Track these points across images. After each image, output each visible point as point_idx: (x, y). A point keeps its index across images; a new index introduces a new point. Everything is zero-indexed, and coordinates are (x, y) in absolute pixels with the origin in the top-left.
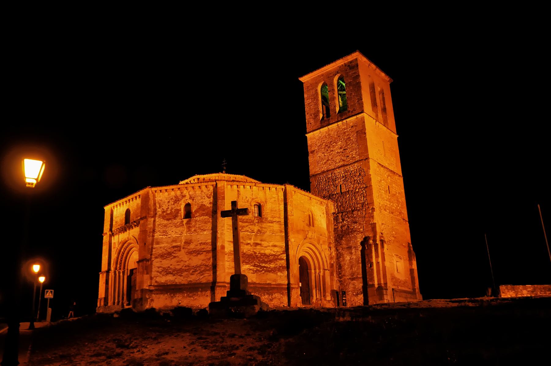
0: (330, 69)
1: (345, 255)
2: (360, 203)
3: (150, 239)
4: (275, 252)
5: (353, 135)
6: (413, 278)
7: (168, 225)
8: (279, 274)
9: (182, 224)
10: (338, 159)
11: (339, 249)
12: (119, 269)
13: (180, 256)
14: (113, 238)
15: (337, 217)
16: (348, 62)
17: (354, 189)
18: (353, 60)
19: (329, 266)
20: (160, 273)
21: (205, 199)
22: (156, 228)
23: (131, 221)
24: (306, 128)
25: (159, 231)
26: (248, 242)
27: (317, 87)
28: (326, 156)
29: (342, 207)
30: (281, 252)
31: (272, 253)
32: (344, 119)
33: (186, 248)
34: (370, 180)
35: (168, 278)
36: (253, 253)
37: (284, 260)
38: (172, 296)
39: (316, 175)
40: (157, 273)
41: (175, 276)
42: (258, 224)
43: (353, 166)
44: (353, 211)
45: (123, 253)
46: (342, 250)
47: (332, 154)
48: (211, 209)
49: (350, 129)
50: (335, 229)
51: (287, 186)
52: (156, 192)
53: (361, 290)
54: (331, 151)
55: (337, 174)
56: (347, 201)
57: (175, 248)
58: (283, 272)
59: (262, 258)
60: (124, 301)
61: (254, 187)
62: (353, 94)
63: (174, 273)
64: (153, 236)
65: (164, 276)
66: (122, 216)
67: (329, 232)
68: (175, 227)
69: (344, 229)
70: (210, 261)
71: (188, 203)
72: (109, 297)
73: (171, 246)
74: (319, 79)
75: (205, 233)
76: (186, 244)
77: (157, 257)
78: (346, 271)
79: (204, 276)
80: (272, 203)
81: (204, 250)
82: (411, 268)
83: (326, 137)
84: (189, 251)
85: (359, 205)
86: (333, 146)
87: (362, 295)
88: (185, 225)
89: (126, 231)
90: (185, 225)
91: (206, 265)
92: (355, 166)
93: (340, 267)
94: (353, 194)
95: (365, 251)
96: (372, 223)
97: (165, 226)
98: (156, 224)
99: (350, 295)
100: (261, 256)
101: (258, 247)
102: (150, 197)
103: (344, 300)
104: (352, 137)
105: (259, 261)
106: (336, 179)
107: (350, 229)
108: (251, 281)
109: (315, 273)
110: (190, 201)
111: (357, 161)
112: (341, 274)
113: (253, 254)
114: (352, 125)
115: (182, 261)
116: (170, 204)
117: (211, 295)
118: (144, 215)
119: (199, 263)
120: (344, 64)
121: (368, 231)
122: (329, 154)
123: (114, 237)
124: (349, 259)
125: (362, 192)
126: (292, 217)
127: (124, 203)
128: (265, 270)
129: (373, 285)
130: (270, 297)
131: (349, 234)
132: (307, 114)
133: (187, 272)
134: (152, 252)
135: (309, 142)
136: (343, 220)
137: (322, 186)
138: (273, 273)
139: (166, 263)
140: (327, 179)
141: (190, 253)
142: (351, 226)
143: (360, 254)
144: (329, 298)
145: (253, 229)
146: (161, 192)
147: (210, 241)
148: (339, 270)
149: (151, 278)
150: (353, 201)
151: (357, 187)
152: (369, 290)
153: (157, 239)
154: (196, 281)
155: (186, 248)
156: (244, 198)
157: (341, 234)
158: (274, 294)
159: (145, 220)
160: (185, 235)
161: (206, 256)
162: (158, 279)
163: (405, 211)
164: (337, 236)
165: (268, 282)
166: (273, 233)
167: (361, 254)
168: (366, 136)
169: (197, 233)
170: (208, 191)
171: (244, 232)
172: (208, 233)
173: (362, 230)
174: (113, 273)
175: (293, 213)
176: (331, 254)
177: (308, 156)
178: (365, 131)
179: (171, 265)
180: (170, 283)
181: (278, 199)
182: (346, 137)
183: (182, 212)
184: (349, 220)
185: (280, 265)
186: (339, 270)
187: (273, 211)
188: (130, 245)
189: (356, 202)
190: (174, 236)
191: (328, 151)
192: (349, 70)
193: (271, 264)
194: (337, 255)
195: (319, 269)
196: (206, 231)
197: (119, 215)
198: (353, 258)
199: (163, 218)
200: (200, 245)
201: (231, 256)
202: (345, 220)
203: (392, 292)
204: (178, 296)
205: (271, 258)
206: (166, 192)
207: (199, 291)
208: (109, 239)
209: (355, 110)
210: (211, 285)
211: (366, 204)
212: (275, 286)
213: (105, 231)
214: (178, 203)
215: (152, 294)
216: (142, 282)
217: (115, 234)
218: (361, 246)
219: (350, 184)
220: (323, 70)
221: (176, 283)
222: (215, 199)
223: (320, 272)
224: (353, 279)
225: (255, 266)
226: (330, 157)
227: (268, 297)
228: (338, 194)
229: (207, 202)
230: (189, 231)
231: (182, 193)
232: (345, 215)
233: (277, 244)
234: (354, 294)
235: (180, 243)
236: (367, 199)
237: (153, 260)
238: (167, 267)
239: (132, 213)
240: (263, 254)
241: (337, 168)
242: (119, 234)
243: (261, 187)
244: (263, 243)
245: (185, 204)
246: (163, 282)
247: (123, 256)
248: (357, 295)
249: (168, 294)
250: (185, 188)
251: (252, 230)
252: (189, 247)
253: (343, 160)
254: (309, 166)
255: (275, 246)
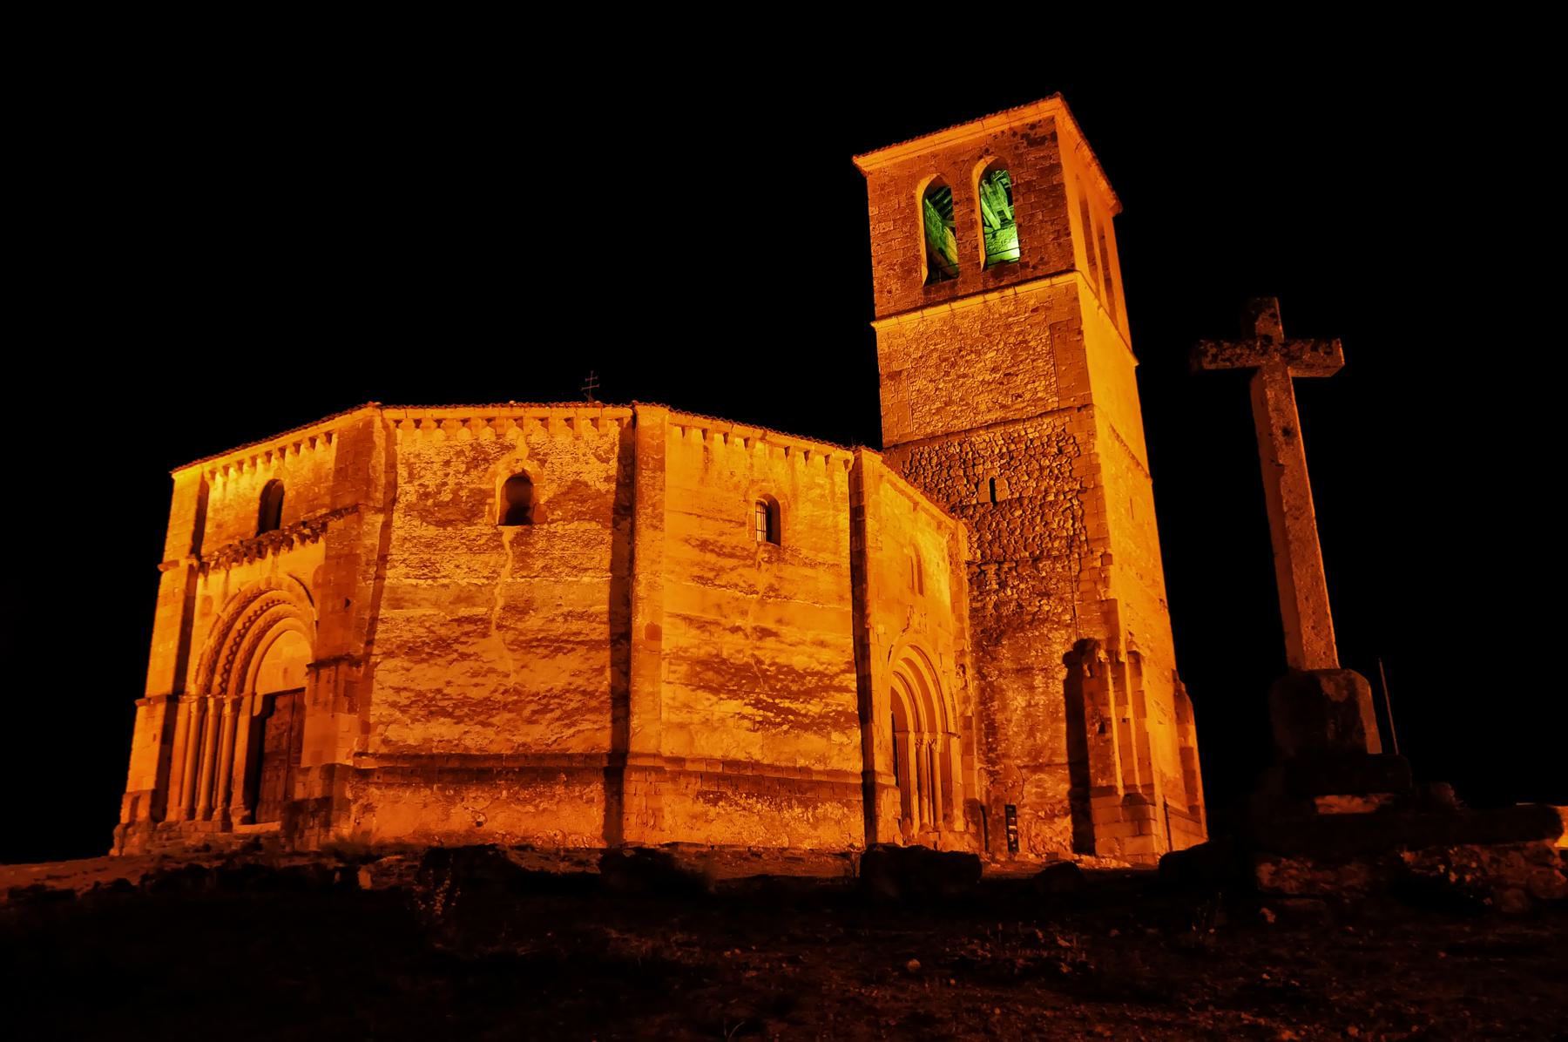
0: (960, 141)
1: (1010, 694)
2: (1062, 538)
3: (367, 587)
4: (822, 664)
5: (1038, 335)
6: (1188, 774)
7: (440, 541)
8: (836, 737)
9: (496, 544)
10: (984, 401)
11: (989, 674)
12: (219, 689)
13: (484, 655)
14: (200, 581)
15: (980, 574)
16: (1023, 125)
17: (1039, 492)
18: (1040, 121)
19: (960, 724)
20: (404, 710)
21: (587, 463)
22: (392, 551)
23: (286, 522)
24: (872, 305)
25: (405, 560)
26: (737, 624)
27: (915, 187)
28: (941, 389)
29: (997, 544)
30: (843, 667)
31: (812, 666)
32: (1008, 287)
33: (508, 628)
34: (1096, 469)
35: (434, 731)
36: (752, 661)
37: (852, 691)
38: (448, 797)
39: (904, 444)
40: (391, 711)
41: (462, 725)
42: (768, 566)
43: (1035, 424)
44: (1036, 560)
45: (242, 636)
46: (1000, 675)
47: (962, 385)
48: (611, 498)
49: (1027, 315)
50: (973, 611)
51: (866, 454)
52: (397, 426)
53: (1066, 803)
54: (959, 377)
55: (981, 447)
56: (1016, 529)
57: (465, 626)
58: (847, 732)
59: (782, 680)
60: (231, 808)
61: (759, 445)
62: (1041, 218)
63: (458, 713)
64: (380, 578)
65: (419, 720)
66: (248, 504)
67: (960, 619)
68: (471, 550)
69: (1005, 611)
70: (602, 677)
71: (524, 471)
72: (174, 791)
73: (448, 618)
74: (922, 166)
75: (586, 579)
76: (509, 614)
77: (393, 652)
78: (1014, 743)
79: (579, 731)
80: (814, 504)
81: (581, 638)
82: (1183, 745)
83: (942, 334)
84: (522, 638)
85: (1058, 542)
86: (967, 361)
87: (1069, 818)
88: (507, 545)
89: (261, 555)
90: (507, 545)
91: (584, 693)
92: (1045, 426)
93: (992, 729)
94: (1037, 509)
95: (1083, 682)
96: (1104, 599)
97: (428, 546)
98: (394, 537)
99: (1027, 817)
100: (779, 671)
101: (770, 642)
102: (376, 439)
103: (1009, 831)
104: (1034, 338)
105: (772, 688)
106: (976, 462)
107: (1027, 614)
108: (745, 754)
109: (920, 742)
110: (531, 467)
111: (1052, 412)
112: (996, 749)
113: (751, 665)
114: (1034, 305)
115: (492, 671)
116: (451, 471)
117: (607, 800)
118: (348, 500)
119: (559, 684)
120: (1011, 129)
121: (1088, 622)
122: (954, 386)
123: (206, 576)
124: (1024, 704)
125: (1068, 505)
126: (878, 555)
127: (259, 461)
128: (792, 721)
129: (1111, 790)
130: (809, 815)
131: (1022, 629)
132: (879, 263)
133: (510, 711)
134: (375, 632)
135: (882, 347)
136: (1003, 585)
137: (925, 477)
138: (815, 732)
139: (427, 677)
140: (944, 459)
141: (526, 645)
142: (1030, 605)
143: (1062, 692)
144: (959, 825)
145: (752, 582)
146: (417, 427)
147: (605, 607)
148: (987, 738)
149: (366, 728)
150: (1037, 528)
151: (1051, 487)
152: (1099, 808)
153: (393, 589)
154: (547, 745)
155: (508, 628)
156: (726, 473)
157: (994, 626)
158: (822, 804)
159: (354, 517)
160: (507, 581)
161: (588, 659)
162: (393, 733)
163: (1159, 576)
164: (982, 632)
165: (801, 762)
166: (816, 600)
167: (1065, 691)
168: (1082, 340)
169: (553, 579)
170: (601, 437)
171: (723, 587)
172: (596, 580)
173: (1067, 617)
174: (194, 706)
175: (881, 542)
176: (966, 686)
177: (877, 386)
178: (1081, 323)
179: (448, 683)
180: (443, 748)
181: (833, 493)
182: (1012, 340)
183: (497, 503)
184: (1022, 586)
185: (840, 709)
186: (987, 738)
187: (817, 528)
188: (272, 610)
189: (1048, 533)
190: (463, 583)
191: (948, 376)
192: (1025, 148)
193: (809, 703)
194: (982, 691)
195: (933, 730)
196: (590, 573)
197: (231, 500)
198: (1037, 705)
199: (423, 519)
200: (566, 620)
201: (679, 665)
202: (1008, 585)
203: (1163, 812)
204: (474, 798)
205: (810, 682)
206: (439, 427)
207: (558, 784)
208: (188, 583)
209: (1046, 263)
210: (605, 764)
211: (1081, 542)
212: (824, 778)
213: (168, 556)
214: (486, 470)
215: (368, 784)
216: (329, 741)
217: (214, 568)
218: (1067, 666)
219: (1026, 478)
220: (936, 142)
221: (466, 748)
222: (624, 466)
223: (935, 741)
224: (1037, 768)
225: (760, 706)
226: (957, 395)
227: (803, 813)
228: (983, 505)
229: (594, 475)
230: (522, 568)
231: (498, 436)
232: (1010, 569)
233: (829, 637)
234: (1039, 816)
235: (485, 610)
236: (1085, 527)
237: (376, 664)
238: (430, 691)
239: (290, 494)
240: (785, 666)
241: (980, 428)
242: (230, 567)
243: (779, 446)
244: (784, 630)
245: (510, 475)
246: (411, 742)
247: (238, 645)
248: (1051, 817)
249: (432, 789)
250: (512, 421)
251: (750, 586)
252: (520, 626)
253: (1003, 407)
254: (881, 417)
255: (823, 644)
